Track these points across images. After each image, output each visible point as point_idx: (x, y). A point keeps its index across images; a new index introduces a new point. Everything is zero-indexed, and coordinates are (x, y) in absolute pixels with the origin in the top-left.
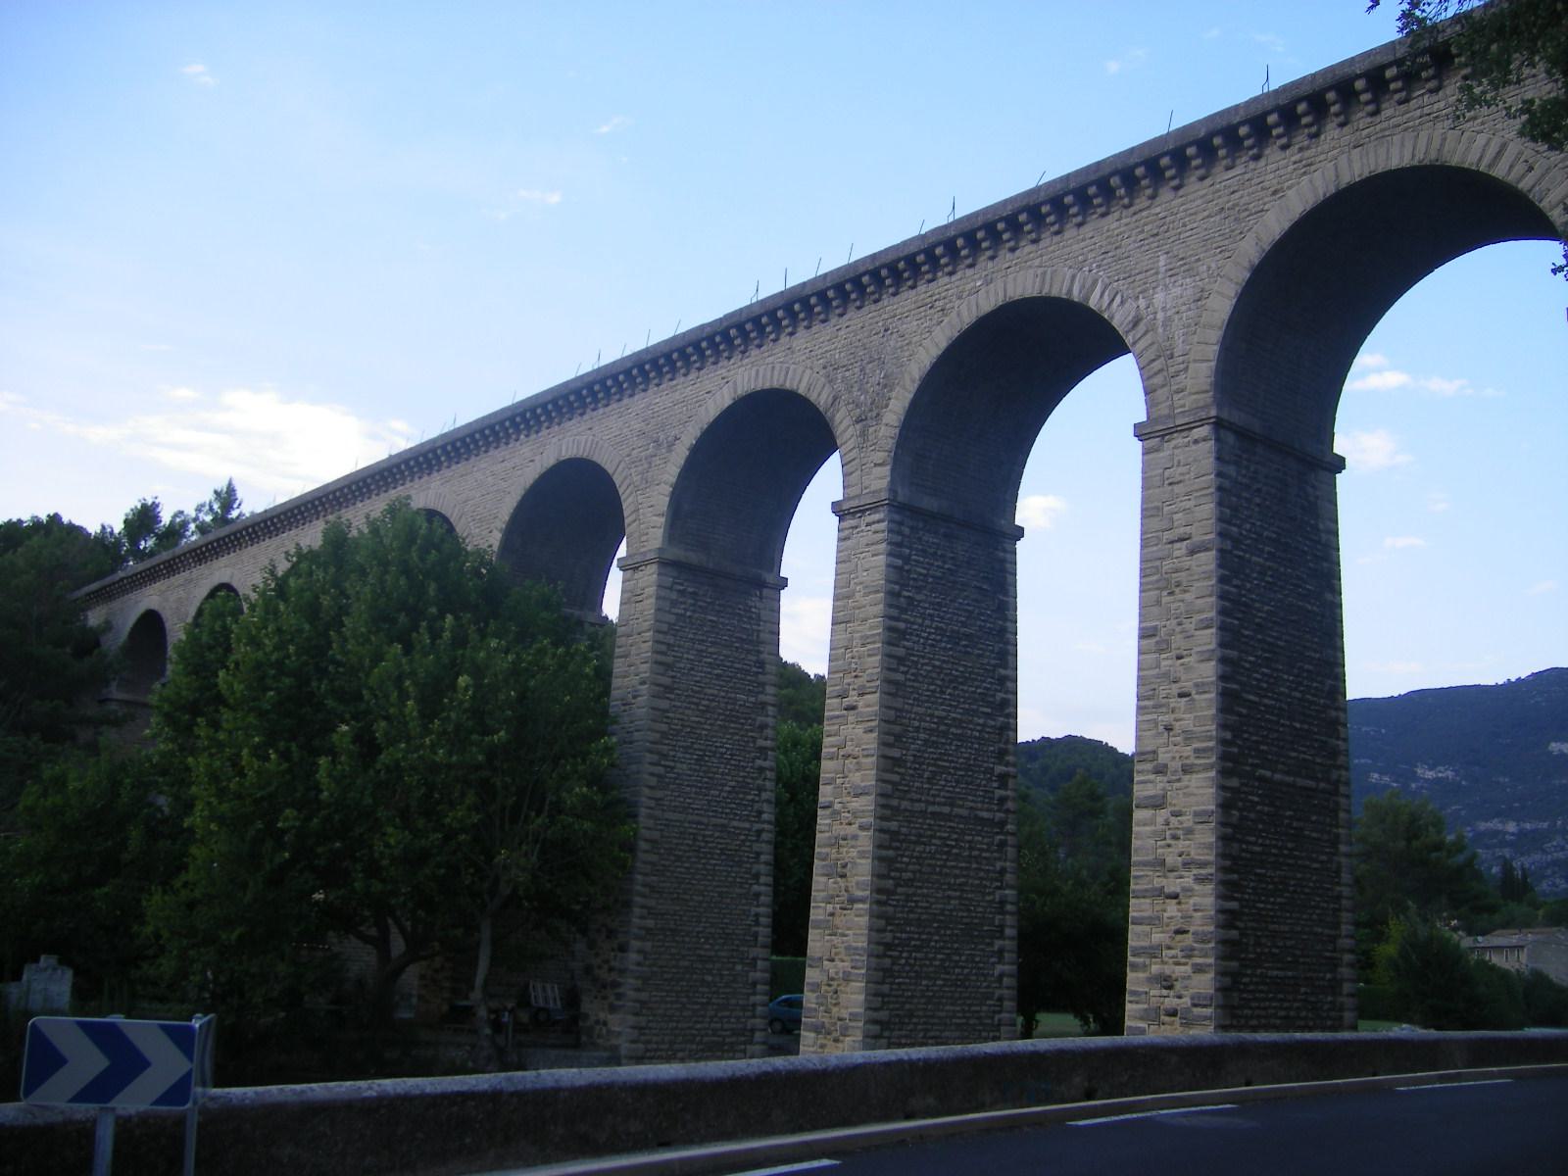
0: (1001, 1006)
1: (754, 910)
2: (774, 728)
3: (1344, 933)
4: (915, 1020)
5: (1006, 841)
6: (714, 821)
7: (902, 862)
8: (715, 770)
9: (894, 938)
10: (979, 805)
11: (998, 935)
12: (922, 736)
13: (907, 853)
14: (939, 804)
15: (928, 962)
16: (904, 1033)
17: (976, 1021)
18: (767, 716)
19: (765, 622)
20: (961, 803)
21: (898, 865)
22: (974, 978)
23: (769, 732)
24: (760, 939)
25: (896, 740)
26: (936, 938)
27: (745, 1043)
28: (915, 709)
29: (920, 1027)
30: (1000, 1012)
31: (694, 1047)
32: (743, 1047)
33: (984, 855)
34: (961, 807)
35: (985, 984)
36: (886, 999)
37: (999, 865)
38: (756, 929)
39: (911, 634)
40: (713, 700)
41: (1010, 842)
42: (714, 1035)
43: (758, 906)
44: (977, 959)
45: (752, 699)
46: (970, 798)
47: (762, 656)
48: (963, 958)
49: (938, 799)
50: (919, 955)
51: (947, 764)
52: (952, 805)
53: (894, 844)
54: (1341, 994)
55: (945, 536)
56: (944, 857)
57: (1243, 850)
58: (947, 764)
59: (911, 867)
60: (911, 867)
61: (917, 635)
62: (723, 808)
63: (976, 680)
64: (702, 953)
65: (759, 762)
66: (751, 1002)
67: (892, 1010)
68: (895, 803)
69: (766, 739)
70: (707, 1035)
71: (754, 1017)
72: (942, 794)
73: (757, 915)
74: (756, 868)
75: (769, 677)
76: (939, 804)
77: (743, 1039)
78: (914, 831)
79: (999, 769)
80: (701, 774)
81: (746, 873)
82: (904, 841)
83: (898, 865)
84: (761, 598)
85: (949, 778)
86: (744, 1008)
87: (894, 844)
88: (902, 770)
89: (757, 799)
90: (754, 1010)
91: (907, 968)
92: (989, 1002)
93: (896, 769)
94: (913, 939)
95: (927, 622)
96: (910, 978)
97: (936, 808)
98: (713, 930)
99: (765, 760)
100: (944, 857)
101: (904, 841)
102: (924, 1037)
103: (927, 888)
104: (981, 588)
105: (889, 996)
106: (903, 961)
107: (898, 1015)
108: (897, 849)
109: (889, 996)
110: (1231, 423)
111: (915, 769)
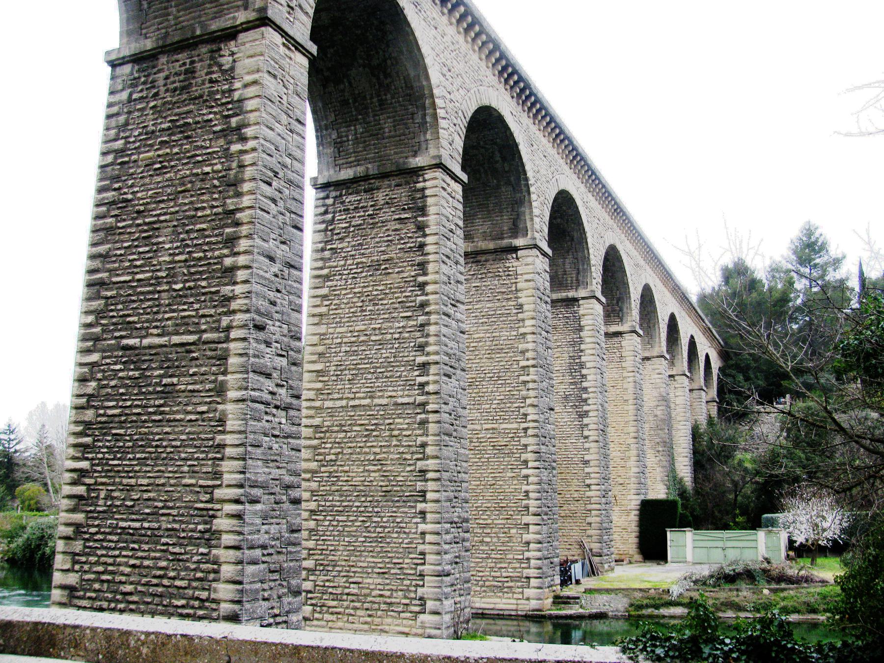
0: (424, 559)
1: (525, 488)
2: (534, 350)
3: (225, 483)
4: (338, 568)
5: (428, 418)
6: (485, 426)
7: (324, 448)
8: (484, 390)
9: (319, 506)
10: (400, 393)
11: (420, 499)
12: (343, 349)
13: (329, 440)
14: (360, 398)
15: (350, 524)
16: (329, 578)
17: (398, 572)
18: (527, 342)
19: (521, 275)
20: (380, 394)
21: (323, 451)
22: (395, 535)
23: (529, 355)
24: (531, 509)
25: (319, 358)
26: (357, 504)
27: (522, 587)
28: (338, 330)
29: (342, 574)
30: (424, 564)
31: (478, 589)
32: (520, 590)
33: (404, 433)
34: (382, 397)
35: (406, 541)
36: (311, 552)
37: (420, 440)
38: (526, 502)
39: (335, 275)
40: (480, 342)
41: (430, 420)
42: (493, 581)
43: (528, 484)
44: (398, 520)
45: (515, 333)
46: (390, 389)
47: (520, 300)
48: (385, 519)
49: (357, 395)
50: (340, 518)
51: (368, 366)
52: (371, 397)
53: (317, 435)
54: (217, 547)
55: (366, 191)
56: (364, 440)
57: (101, 415)
58: (368, 366)
59: (333, 451)
60: (333, 451)
61: (340, 274)
62: (493, 416)
63: (396, 293)
64: (481, 522)
65: (522, 378)
66: (525, 557)
67: (316, 560)
68: (318, 404)
69: (528, 360)
70: (488, 580)
71: (529, 568)
72: (363, 390)
73: (527, 492)
74: (524, 457)
75: (526, 314)
76: (360, 398)
77: (520, 584)
78: (336, 423)
79: (421, 359)
80: (473, 395)
81: (516, 461)
82: (327, 431)
83: (323, 451)
84: (517, 258)
85: (369, 376)
86: (520, 561)
87: (317, 435)
88: (326, 379)
89: (522, 405)
90: (529, 563)
91: (331, 528)
92: (411, 556)
93: (321, 378)
94: (335, 506)
95: (349, 262)
96: (334, 536)
97: (357, 402)
98: (489, 505)
99: (528, 375)
100: (364, 440)
101: (327, 431)
102: (347, 582)
103: (348, 465)
104: (400, 219)
105: (313, 549)
106: (327, 523)
107: (322, 565)
108: (320, 438)
109: (313, 549)
110: (124, 58)
111: (337, 375)
